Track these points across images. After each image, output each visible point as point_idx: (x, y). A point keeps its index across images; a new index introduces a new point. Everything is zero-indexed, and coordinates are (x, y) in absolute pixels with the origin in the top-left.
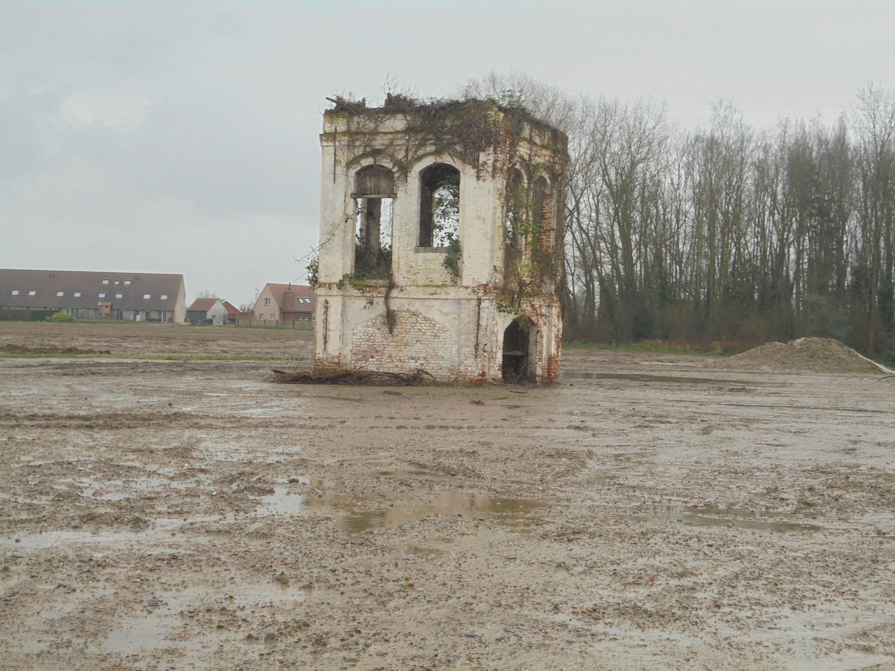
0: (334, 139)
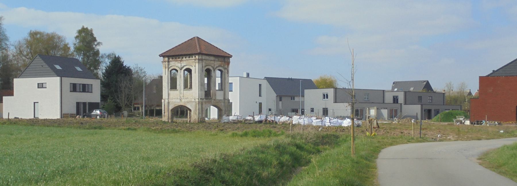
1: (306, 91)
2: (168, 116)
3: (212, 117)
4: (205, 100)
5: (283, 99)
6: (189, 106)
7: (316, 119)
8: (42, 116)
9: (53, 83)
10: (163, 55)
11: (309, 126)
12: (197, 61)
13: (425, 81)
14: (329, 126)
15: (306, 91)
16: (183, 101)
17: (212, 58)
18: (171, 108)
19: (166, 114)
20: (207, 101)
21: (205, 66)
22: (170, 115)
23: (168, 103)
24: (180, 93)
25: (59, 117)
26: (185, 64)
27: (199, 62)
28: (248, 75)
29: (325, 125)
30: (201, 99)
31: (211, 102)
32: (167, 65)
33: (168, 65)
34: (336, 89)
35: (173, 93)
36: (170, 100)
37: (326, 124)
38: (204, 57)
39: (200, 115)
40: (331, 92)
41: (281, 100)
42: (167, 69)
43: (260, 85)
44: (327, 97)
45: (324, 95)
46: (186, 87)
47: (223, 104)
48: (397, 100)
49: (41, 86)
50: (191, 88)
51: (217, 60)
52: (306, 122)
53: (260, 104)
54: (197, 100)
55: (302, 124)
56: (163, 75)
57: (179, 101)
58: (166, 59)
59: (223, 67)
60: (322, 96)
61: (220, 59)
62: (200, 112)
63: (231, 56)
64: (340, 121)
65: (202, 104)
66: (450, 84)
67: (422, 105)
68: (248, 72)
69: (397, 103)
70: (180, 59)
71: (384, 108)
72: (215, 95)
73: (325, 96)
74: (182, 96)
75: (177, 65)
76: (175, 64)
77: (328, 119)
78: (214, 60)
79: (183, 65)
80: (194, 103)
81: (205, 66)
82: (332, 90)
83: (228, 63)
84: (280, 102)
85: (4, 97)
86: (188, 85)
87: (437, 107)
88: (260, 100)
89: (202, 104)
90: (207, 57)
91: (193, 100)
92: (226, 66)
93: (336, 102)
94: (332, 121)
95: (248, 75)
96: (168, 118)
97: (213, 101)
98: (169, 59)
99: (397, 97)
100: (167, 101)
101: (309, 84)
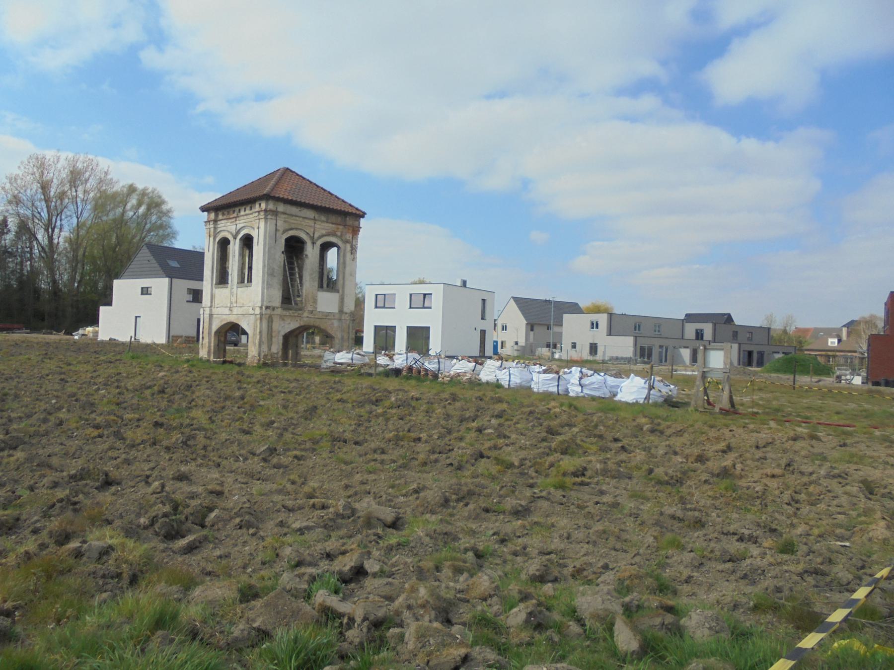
0: (276, 215)
1: (566, 317)
2: (209, 347)
3: (201, 355)
4: (279, 311)
5: (535, 328)
6: (244, 325)
7: (545, 372)
8: (145, 338)
9: (160, 285)
10: (204, 209)
11: (525, 390)
12: (262, 215)
13: (725, 314)
14: (577, 398)
15: (566, 317)
16: (235, 311)
17: (310, 213)
18: (215, 328)
19: (206, 341)
20: (285, 313)
21: (285, 231)
22: (212, 344)
23: (211, 316)
24: (232, 293)
25: (162, 340)
26: (242, 225)
27: (266, 219)
28: (464, 283)
29: (567, 391)
30: (267, 308)
31: (300, 316)
32: (212, 230)
33: (215, 228)
34: (611, 315)
35: (222, 293)
36: (215, 311)
37: (570, 388)
38: (281, 207)
39: (265, 348)
40: (603, 319)
41: (532, 330)
42: (212, 239)
43: (484, 301)
44: (597, 327)
45: (593, 324)
46: (241, 281)
47: (336, 323)
48: (702, 335)
49: (145, 291)
50: (250, 280)
51: (323, 218)
52: (516, 380)
53: (483, 332)
54: (258, 311)
55: (505, 384)
56: (206, 251)
57: (227, 311)
58: (213, 216)
59: (341, 237)
60: (589, 325)
61: (333, 218)
62: (265, 338)
63: (363, 215)
64: (611, 380)
65: (270, 320)
66: (771, 316)
67: (740, 344)
68: (465, 279)
69: (702, 339)
70: (235, 215)
71: (685, 347)
72: (315, 301)
73: (595, 325)
74: (234, 300)
75: (229, 229)
76: (228, 227)
77: (578, 375)
78: (314, 219)
79: (239, 226)
80: (252, 317)
81: (285, 231)
82: (605, 316)
83: (356, 230)
84: (532, 333)
85: (101, 308)
86: (246, 278)
87: (761, 348)
88: (483, 325)
89: (270, 320)
90: (294, 210)
91: (251, 312)
92: (349, 236)
93: (610, 335)
94: (586, 381)
95: (464, 283)
96: (209, 352)
97: (305, 314)
98: (217, 215)
99: (702, 330)
100: (207, 311)
101: (574, 308)
